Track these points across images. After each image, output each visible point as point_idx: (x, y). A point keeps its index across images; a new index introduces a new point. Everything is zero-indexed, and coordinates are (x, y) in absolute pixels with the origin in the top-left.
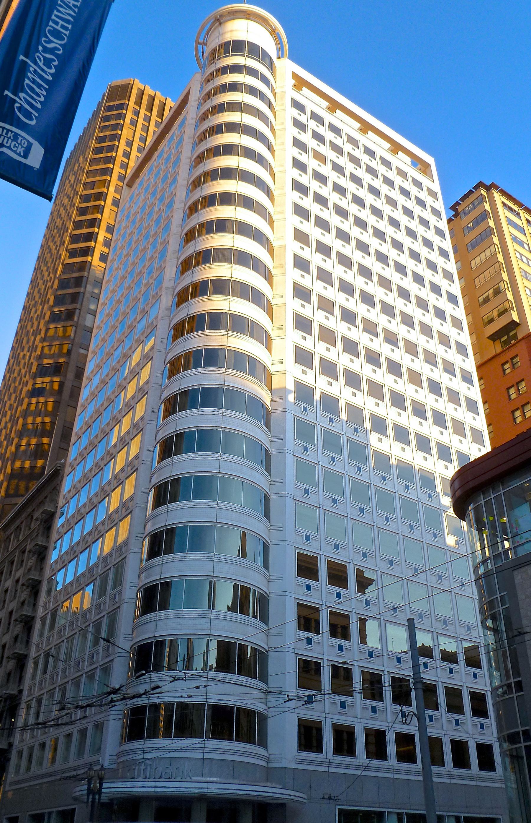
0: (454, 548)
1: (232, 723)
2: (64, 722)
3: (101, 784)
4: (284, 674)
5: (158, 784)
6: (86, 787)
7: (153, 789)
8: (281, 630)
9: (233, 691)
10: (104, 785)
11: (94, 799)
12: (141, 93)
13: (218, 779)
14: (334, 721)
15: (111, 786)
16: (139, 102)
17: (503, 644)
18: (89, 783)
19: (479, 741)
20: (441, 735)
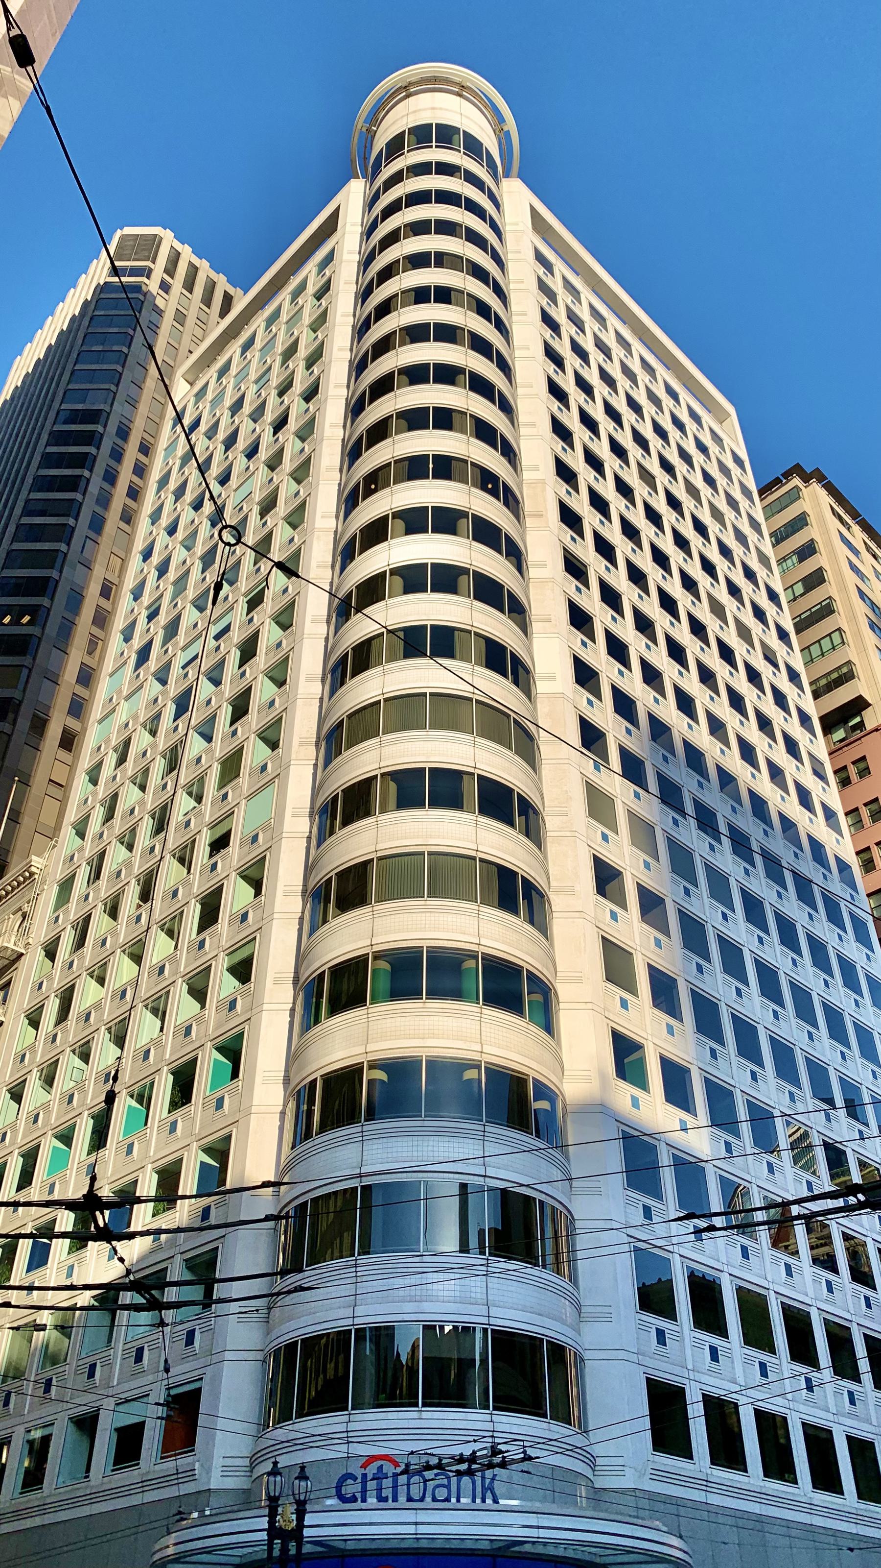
0: (152, 1252)
1: (529, 1372)
2: (187, 1200)
3: (301, 1514)
4: (608, 1277)
5: (422, 1516)
6: (264, 1523)
7: (411, 1529)
8: (597, 1184)
9: (509, 1299)
10: (309, 1519)
11: (284, 1549)
12: (175, 258)
13: (538, 1504)
14: (650, 1371)
15: (192, 1251)
16: (170, 270)
17: (569, 1256)
18: (272, 1515)
19: (854, 1432)
20: (787, 1411)
